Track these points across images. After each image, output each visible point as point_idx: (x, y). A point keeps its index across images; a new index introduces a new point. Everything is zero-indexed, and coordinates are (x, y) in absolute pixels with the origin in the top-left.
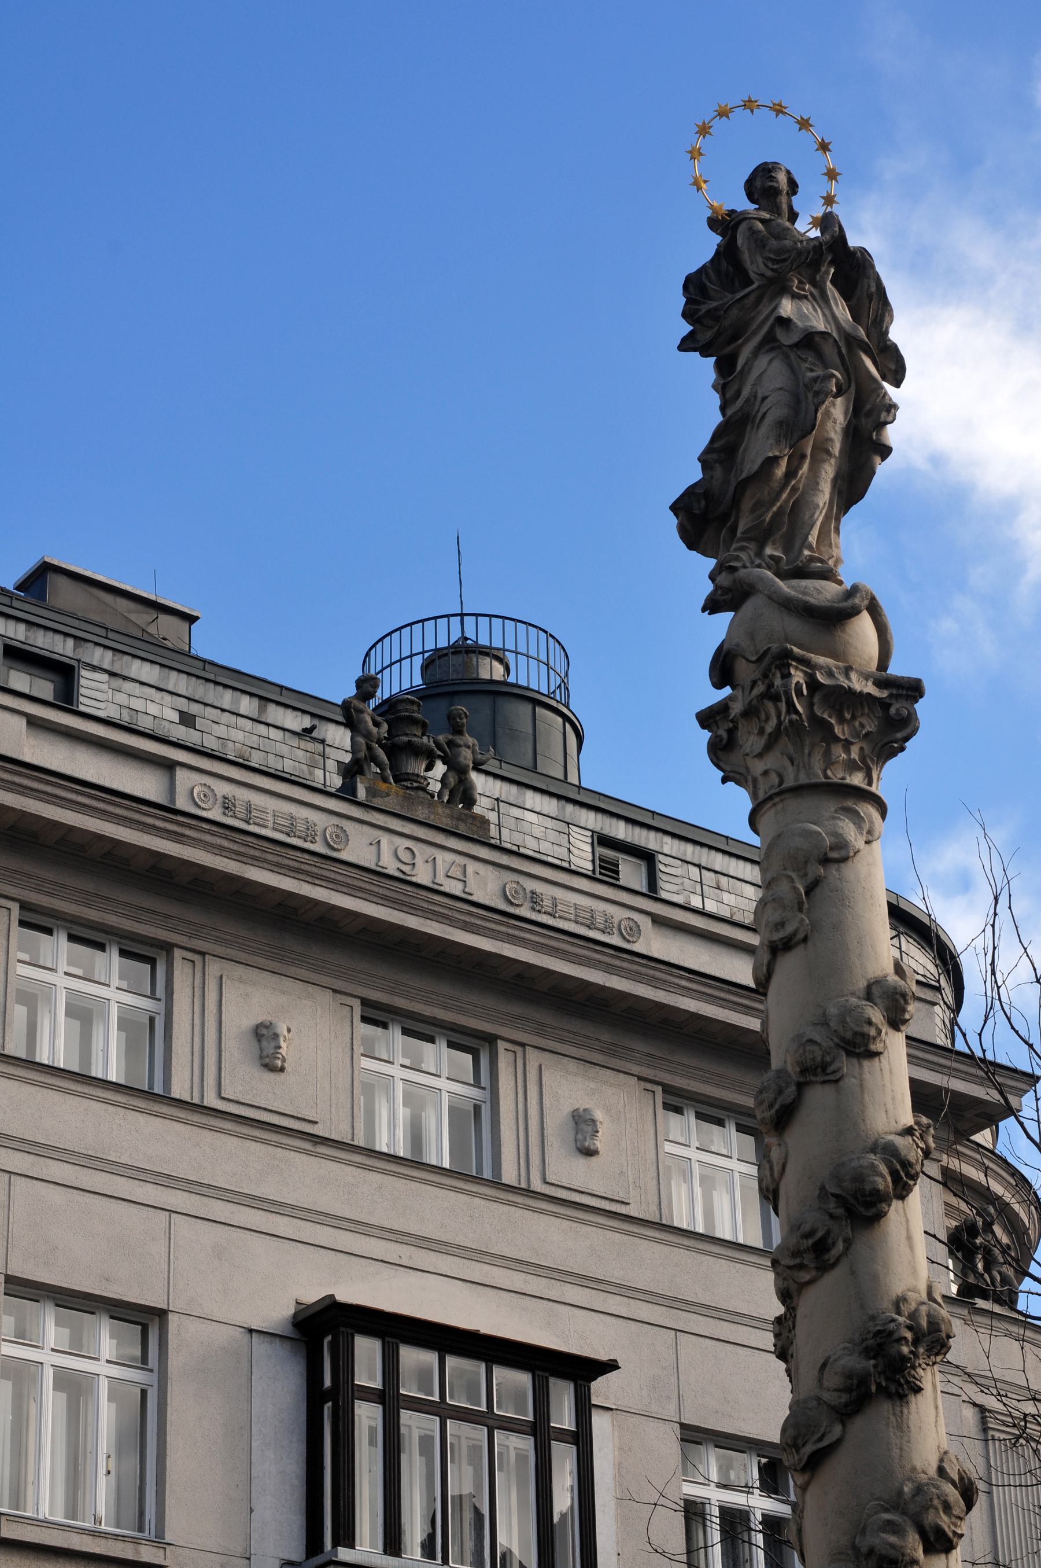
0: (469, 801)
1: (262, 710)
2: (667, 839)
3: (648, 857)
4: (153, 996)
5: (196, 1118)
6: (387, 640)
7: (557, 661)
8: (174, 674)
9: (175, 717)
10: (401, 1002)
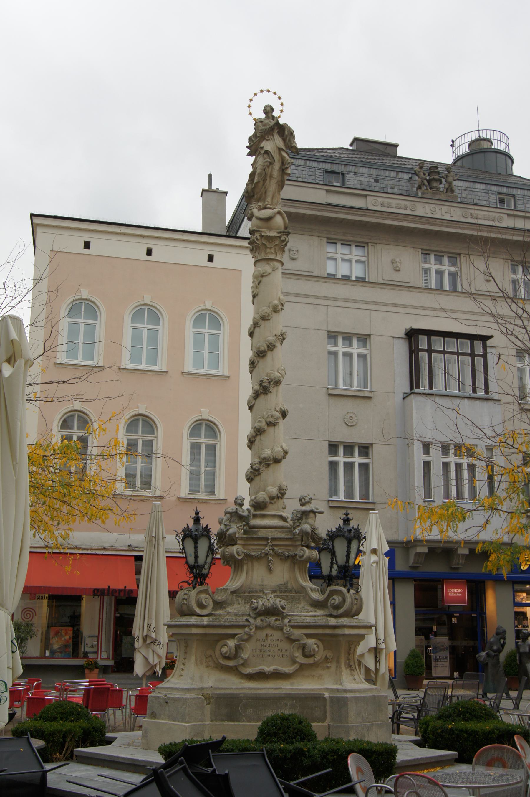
0: (452, 191)
1: (397, 174)
2: (519, 190)
3: (514, 196)
4: (365, 256)
5: (378, 286)
6: (458, 139)
7: (504, 138)
8: (372, 169)
9: (373, 181)
10: (432, 248)
